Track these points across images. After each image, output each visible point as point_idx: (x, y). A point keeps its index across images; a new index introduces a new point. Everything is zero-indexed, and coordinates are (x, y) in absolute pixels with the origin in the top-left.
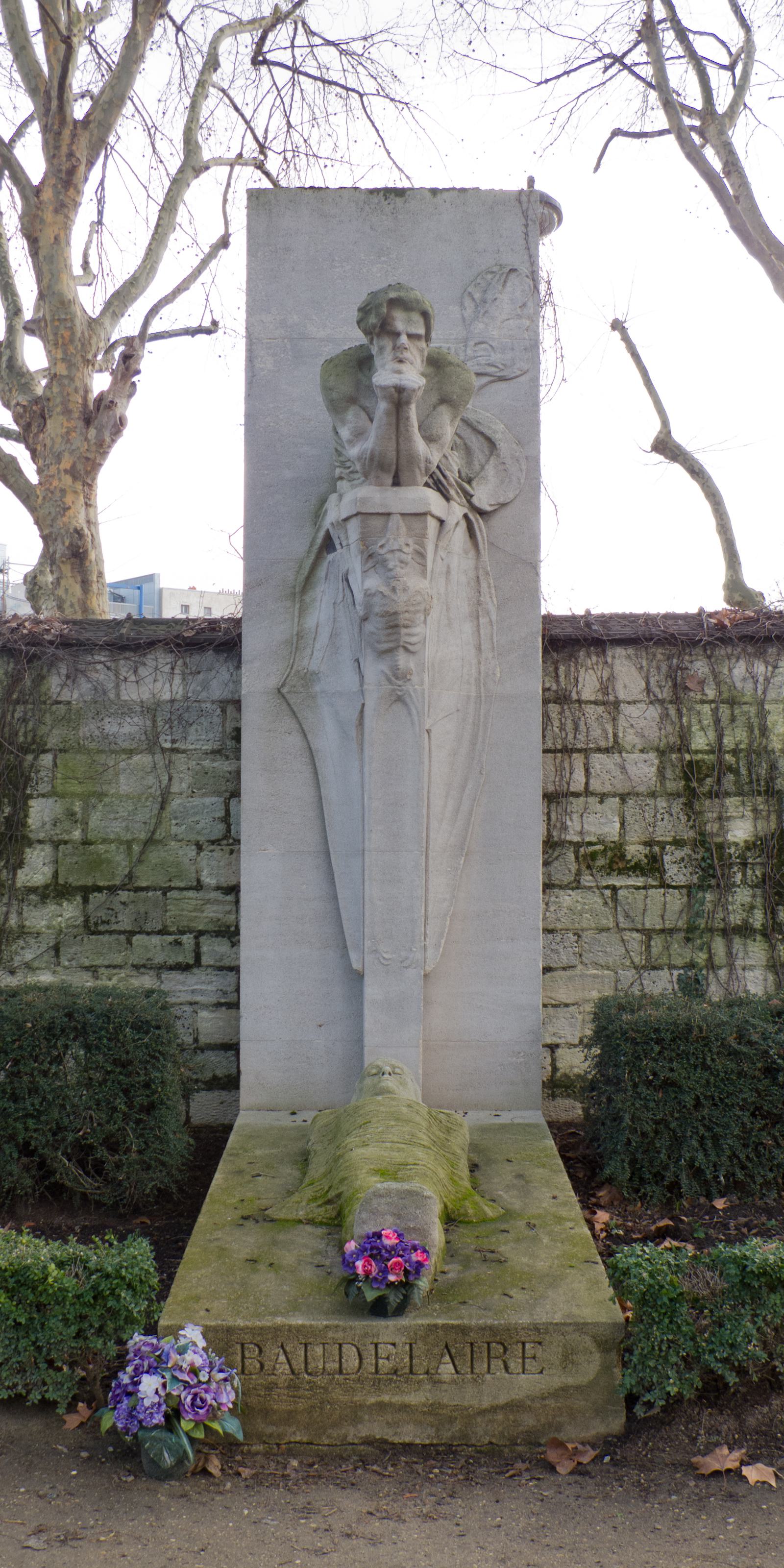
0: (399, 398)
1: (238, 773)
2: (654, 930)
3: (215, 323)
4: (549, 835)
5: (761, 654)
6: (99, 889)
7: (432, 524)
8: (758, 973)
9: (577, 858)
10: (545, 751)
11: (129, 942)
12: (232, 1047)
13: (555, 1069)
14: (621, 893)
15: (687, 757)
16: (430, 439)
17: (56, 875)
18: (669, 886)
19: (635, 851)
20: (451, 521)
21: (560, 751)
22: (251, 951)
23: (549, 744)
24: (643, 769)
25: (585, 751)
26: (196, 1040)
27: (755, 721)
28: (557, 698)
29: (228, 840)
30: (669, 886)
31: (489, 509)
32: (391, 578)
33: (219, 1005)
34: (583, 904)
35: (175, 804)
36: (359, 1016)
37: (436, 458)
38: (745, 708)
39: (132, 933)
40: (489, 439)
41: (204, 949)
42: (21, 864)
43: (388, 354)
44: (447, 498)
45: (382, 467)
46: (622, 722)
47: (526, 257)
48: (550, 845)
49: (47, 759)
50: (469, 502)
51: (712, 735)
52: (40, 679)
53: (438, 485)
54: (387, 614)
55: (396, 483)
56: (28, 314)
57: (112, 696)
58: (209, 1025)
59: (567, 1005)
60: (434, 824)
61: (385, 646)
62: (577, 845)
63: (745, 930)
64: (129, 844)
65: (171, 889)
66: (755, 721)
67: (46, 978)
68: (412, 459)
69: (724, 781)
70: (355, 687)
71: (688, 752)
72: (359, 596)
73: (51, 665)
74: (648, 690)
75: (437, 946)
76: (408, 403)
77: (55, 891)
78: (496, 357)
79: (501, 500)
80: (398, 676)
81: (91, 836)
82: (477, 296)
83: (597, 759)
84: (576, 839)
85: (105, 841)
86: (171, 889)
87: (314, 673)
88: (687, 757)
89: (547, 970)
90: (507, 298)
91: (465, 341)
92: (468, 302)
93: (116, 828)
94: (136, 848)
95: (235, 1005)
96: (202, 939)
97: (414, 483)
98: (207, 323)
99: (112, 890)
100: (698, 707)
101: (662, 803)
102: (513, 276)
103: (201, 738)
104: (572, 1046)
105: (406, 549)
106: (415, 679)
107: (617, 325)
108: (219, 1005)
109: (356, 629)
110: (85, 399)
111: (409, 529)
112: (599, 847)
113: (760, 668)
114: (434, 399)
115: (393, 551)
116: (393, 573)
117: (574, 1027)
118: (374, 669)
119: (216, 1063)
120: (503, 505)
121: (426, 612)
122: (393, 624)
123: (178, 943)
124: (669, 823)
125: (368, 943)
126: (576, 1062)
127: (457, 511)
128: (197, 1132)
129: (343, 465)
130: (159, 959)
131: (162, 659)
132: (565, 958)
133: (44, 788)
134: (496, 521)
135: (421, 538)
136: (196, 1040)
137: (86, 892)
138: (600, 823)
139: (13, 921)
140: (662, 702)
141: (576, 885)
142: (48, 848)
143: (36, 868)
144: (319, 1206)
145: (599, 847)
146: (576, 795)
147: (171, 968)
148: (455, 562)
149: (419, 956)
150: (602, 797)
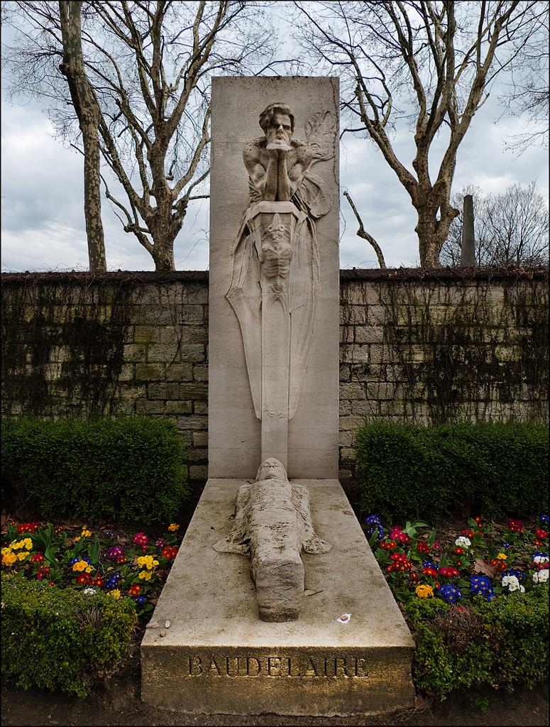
2: (382, 400)
6: (153, 382)
9: (350, 370)
10: (340, 325)
11: (165, 404)
12: (206, 447)
13: (341, 457)
16: (293, 179)
18: (389, 382)
19: (375, 367)
20: (301, 220)
22: (212, 409)
24: (379, 333)
25: (354, 326)
26: (192, 444)
28: (344, 303)
30: (389, 382)
31: (317, 217)
34: (354, 388)
35: (184, 346)
37: (295, 188)
38: (421, 308)
40: (317, 186)
42: (120, 372)
43: (274, 135)
45: (271, 192)
46: (370, 313)
47: (334, 107)
50: (309, 212)
51: (407, 319)
52: (129, 295)
54: (272, 260)
55: (277, 199)
57: (158, 302)
59: (346, 431)
60: (293, 355)
61: (272, 275)
63: (420, 400)
64: (165, 363)
68: (285, 187)
69: (412, 338)
71: (397, 325)
73: (133, 289)
74: (380, 300)
75: (294, 408)
77: (134, 383)
78: (320, 151)
79: (322, 213)
80: (277, 289)
81: (149, 360)
82: (312, 123)
83: (359, 329)
84: (350, 362)
85: (155, 362)
86: (182, 382)
92: (308, 126)
93: (160, 357)
94: (167, 365)
95: (207, 430)
96: (195, 403)
97: (284, 200)
99: (159, 382)
100: (401, 307)
101: (386, 347)
102: (328, 114)
103: (195, 319)
105: (281, 230)
106: (284, 290)
109: (259, 267)
111: (283, 220)
115: (275, 230)
116: (276, 241)
118: (266, 286)
120: (323, 215)
122: (275, 264)
124: (387, 353)
125: (263, 407)
126: (349, 453)
127: (303, 216)
128: (189, 481)
130: (178, 410)
133: (130, 340)
136: (192, 444)
137: (147, 383)
138: (360, 355)
140: (386, 305)
143: (126, 375)
144: (240, 544)
146: (350, 344)
148: (302, 239)
150: (361, 345)
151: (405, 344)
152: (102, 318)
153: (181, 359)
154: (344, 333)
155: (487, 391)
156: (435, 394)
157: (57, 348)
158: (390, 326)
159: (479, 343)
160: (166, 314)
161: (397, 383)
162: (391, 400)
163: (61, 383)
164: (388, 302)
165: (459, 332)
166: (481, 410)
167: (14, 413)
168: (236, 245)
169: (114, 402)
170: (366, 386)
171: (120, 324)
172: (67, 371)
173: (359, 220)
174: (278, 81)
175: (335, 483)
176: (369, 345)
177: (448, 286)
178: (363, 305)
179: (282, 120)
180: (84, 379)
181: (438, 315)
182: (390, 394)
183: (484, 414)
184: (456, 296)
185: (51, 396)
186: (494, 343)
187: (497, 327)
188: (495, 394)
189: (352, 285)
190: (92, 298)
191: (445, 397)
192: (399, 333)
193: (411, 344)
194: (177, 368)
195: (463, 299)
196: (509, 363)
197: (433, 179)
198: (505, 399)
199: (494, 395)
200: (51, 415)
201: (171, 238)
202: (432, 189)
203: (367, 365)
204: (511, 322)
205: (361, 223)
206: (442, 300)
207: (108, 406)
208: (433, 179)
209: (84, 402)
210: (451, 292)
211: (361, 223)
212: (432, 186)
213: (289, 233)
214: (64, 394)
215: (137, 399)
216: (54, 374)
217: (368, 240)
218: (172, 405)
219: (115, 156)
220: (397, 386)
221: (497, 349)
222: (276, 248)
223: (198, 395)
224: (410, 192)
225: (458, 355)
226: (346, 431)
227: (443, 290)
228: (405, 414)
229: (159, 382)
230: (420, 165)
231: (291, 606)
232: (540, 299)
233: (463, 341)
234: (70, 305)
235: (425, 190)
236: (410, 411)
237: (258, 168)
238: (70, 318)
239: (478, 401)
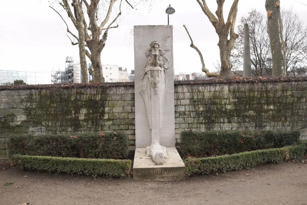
0: (155, 56)
1: (134, 103)
3: (118, 25)
4: (175, 111)
5: (203, 86)
7: (160, 71)
8: (203, 129)
10: (175, 99)
12: (135, 140)
13: (177, 142)
14: (185, 118)
15: (194, 100)
16: (159, 60)
17: (109, 117)
18: (191, 117)
19: (187, 113)
21: (177, 99)
23: (175, 98)
24: (188, 102)
25: (180, 99)
27: (203, 95)
28: (176, 92)
29: (133, 112)
30: (191, 117)
32: (155, 78)
33: (131, 134)
35: (125, 107)
36: (151, 135)
39: (119, 125)
40: (167, 59)
41: (129, 127)
42: (104, 116)
43: (154, 50)
44: (161, 67)
45: (153, 64)
48: (175, 112)
49: (107, 102)
51: (197, 97)
53: (160, 66)
54: (154, 83)
55: (155, 66)
56: (88, 26)
58: (130, 137)
62: (179, 112)
63: (202, 123)
64: (119, 113)
65: (125, 119)
66: (203, 95)
67: (108, 131)
68: (157, 63)
70: (150, 92)
72: (150, 81)
74: (188, 91)
76: (157, 56)
77: (109, 120)
80: (155, 91)
81: (114, 112)
82: (165, 40)
83: (181, 100)
85: (115, 113)
87: (144, 90)
88: (194, 100)
89: (175, 129)
90: (168, 40)
91: (163, 46)
93: (117, 111)
94: (120, 114)
98: (116, 26)
99: (117, 119)
101: (190, 106)
104: (179, 139)
106: (158, 91)
107: (184, 26)
108: (131, 134)
110: (98, 41)
112: (182, 112)
113: (203, 88)
114: (160, 55)
117: (178, 136)
118: (152, 90)
119: (132, 142)
121: (159, 83)
122: (155, 84)
123: (125, 126)
124: (191, 108)
127: (163, 69)
129: (148, 63)
130: (124, 128)
131: (123, 88)
132: (178, 127)
134: (167, 70)
135: (158, 73)
137: (113, 120)
138: (182, 109)
139: (103, 124)
140: (190, 92)
141: (179, 117)
142: (108, 114)
143: (106, 117)
145: (182, 112)
146: (179, 105)
147: (125, 130)
149: (159, 127)
150: (182, 105)
151: (197, 105)
152: (98, 98)
153: (124, 111)
154: (177, 102)
155: (224, 119)
156: (207, 121)
157: (83, 109)
158: (192, 99)
159: (220, 104)
160: (119, 97)
161: (194, 118)
162: (192, 123)
163: (85, 120)
164: (191, 92)
165: (214, 100)
166: (222, 126)
167: (69, 131)
168: (143, 77)
169: (102, 126)
170: (184, 119)
171: (103, 102)
172: (86, 116)
173: (191, 39)
174: (154, 27)
175: (175, 148)
176: (185, 105)
177: (210, 86)
178: (183, 93)
179: (156, 46)
180: (92, 119)
181: (207, 95)
182: (192, 121)
183: (223, 127)
184: (213, 89)
185: (81, 125)
186: (225, 104)
187: (226, 99)
188: (226, 120)
189: (179, 86)
190: (94, 92)
191: (210, 122)
192: (194, 101)
193: (198, 105)
194: (123, 114)
195: (215, 90)
196: (230, 110)
197: (226, 21)
198: (229, 122)
199: (226, 121)
200: (81, 131)
201: (99, 51)
202: (225, 25)
203: (184, 112)
204: (231, 97)
205: (192, 41)
206: (208, 90)
207: (100, 127)
208: (226, 21)
209: (92, 126)
210: (211, 88)
211: (192, 41)
212: (225, 23)
213: (159, 76)
214: (85, 124)
215: (110, 125)
216: (82, 117)
217: (195, 49)
218: (122, 127)
219: (69, 9)
220: (194, 119)
221: (227, 106)
222: (155, 80)
223: (130, 123)
224: (215, 26)
225: (214, 108)
226: (178, 133)
227: (209, 87)
228: (197, 128)
229: (117, 119)
230: (219, 12)
231: (162, 162)
232: (240, 89)
233: (215, 104)
234: (87, 94)
235: (222, 26)
236: (199, 127)
237: (149, 57)
238: (87, 99)
239: (221, 123)
